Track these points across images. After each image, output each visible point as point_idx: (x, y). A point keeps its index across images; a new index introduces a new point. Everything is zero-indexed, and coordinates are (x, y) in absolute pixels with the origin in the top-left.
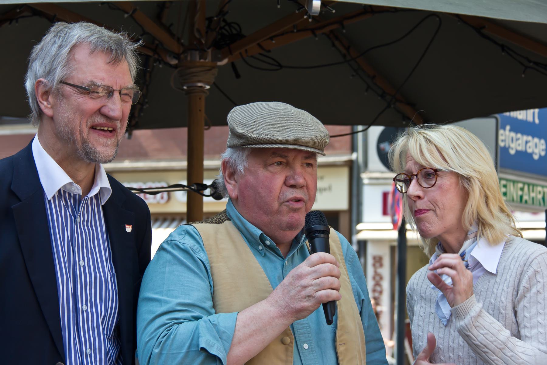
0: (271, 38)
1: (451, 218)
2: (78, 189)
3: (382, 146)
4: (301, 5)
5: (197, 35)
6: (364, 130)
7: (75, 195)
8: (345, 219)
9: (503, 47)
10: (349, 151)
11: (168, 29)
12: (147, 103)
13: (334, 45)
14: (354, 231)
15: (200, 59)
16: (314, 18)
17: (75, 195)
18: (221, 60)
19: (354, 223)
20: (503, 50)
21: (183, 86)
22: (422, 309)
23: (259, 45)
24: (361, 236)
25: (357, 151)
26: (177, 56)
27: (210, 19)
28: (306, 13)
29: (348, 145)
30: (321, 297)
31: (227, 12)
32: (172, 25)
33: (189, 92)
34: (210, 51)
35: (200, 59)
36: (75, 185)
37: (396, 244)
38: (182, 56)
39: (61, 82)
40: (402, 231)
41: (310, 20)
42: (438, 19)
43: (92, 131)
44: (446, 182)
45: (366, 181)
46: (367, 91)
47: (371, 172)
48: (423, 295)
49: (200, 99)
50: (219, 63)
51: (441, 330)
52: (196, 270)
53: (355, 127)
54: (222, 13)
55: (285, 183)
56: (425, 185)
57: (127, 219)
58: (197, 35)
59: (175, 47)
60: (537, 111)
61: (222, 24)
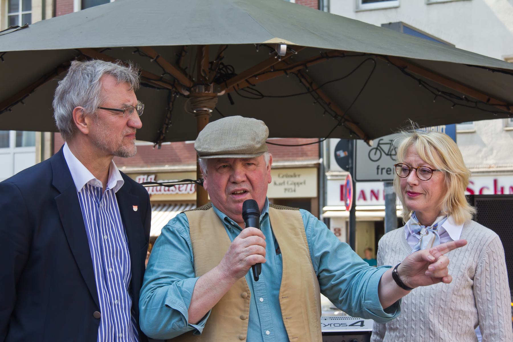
0: (255, 76)
3: (338, 153)
5: (203, 74)
7: (97, 188)
9: (420, 81)
10: (318, 157)
11: (184, 71)
12: (171, 123)
13: (301, 82)
14: (321, 212)
18: (220, 92)
19: (321, 207)
20: (420, 83)
22: (392, 258)
23: (247, 81)
24: (327, 215)
25: (323, 158)
26: (189, 89)
27: (212, 63)
28: (276, 54)
30: (250, 260)
31: (223, 57)
32: (186, 68)
33: (197, 115)
34: (212, 85)
36: (98, 180)
37: (348, 220)
38: (192, 89)
39: (98, 108)
40: (353, 212)
42: (373, 62)
44: (436, 177)
45: (329, 178)
46: (324, 113)
47: (332, 171)
48: (394, 249)
50: (219, 94)
52: (179, 246)
55: (229, 180)
56: (421, 177)
57: (135, 205)
58: (203, 74)
60: (444, 127)
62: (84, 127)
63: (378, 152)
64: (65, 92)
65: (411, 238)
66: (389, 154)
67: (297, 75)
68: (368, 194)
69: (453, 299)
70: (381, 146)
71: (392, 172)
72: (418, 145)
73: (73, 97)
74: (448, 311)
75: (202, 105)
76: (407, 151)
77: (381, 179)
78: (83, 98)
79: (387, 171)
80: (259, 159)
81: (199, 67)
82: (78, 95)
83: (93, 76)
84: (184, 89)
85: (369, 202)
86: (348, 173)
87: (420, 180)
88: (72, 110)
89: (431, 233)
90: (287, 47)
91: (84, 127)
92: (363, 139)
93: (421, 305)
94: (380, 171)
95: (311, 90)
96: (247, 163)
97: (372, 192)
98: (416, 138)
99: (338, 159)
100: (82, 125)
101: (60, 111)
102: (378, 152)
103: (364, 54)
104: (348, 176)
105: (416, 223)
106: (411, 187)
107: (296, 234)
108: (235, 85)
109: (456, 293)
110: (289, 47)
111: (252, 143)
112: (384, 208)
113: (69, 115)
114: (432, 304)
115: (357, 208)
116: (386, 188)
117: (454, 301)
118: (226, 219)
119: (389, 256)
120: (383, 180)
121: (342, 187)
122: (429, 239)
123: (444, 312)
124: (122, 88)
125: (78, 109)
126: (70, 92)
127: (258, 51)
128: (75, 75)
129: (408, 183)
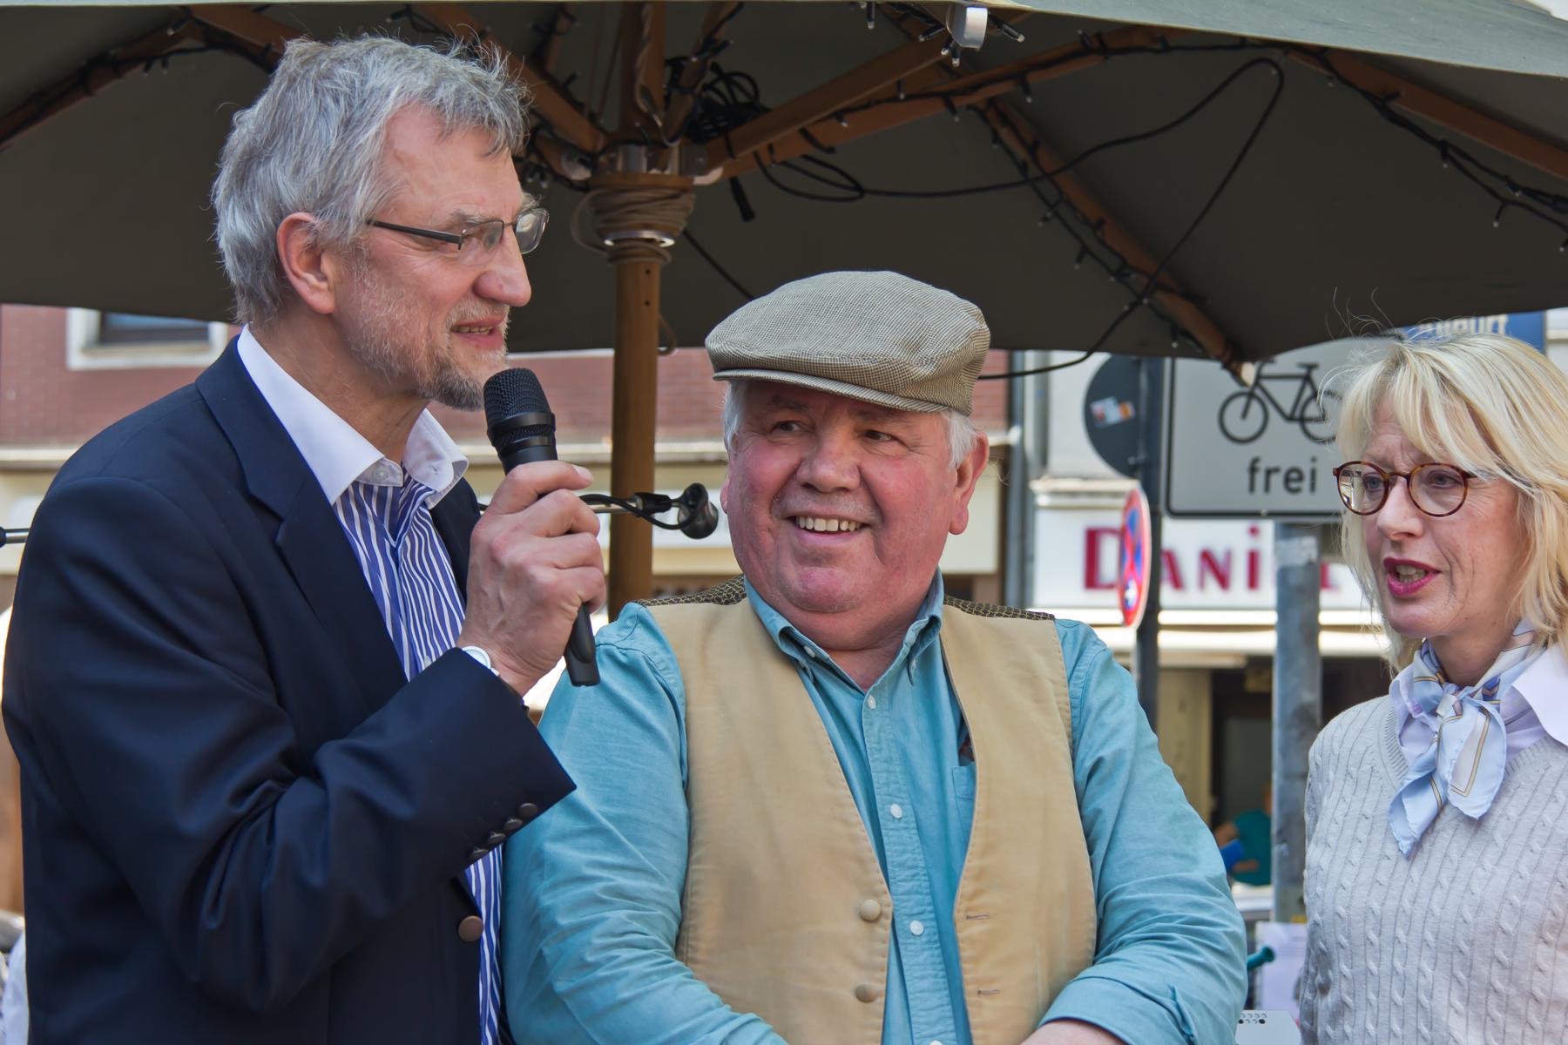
0: (839, 116)
1: (1481, 597)
2: (393, 473)
3: (1098, 407)
4: (931, 20)
6: (1044, 370)
7: (383, 490)
8: (1003, 589)
9: (1444, 148)
10: (1002, 423)
13: (996, 139)
15: (649, 168)
16: (967, 54)
17: (383, 490)
18: (704, 171)
20: (1445, 157)
21: (604, 238)
22: (1342, 806)
23: (804, 133)
25: (1022, 424)
26: (589, 160)
27: (676, 64)
28: (947, 41)
29: (1000, 407)
31: (725, 44)
32: (573, 77)
33: (617, 255)
34: (675, 145)
35: (649, 168)
38: (602, 159)
39: (368, 222)
40: (1148, 632)
41: (956, 62)
42: (1274, 72)
43: (454, 336)
44: (1484, 503)
45: (1043, 500)
46: (1079, 260)
47: (1056, 477)
49: (648, 272)
50: (699, 180)
51: (1385, 862)
53: (1018, 355)
54: (710, 45)
56: (1429, 505)
59: (585, 137)
60: (1502, 319)
61: (710, 76)
62: (318, 290)
63: (1255, 407)
64: (253, 158)
65: (1413, 730)
66: (1298, 417)
67: (983, 115)
68: (1190, 566)
69: (1540, 960)
70: (1267, 384)
71: (1306, 484)
72: (1402, 383)
73: (279, 177)
74: (1519, 1004)
75: (638, 219)
76: (1379, 409)
77: (1264, 511)
78: (314, 185)
79: (1287, 480)
80: (924, 428)
81: (630, 76)
82: (297, 170)
83: (357, 102)
84: (570, 159)
85: (1192, 594)
86: (1131, 485)
87: (1426, 517)
88: (277, 226)
89: (1471, 712)
90: (990, 17)
91: (318, 290)
92: (1218, 358)
93: (1422, 981)
94: (1260, 478)
95: (1034, 171)
96: (872, 424)
97: (1207, 558)
98: (1398, 361)
99: (1103, 438)
100: (312, 278)
101: (234, 225)
102: (1255, 407)
103: (1242, 43)
104: (1131, 499)
105: (1428, 673)
106: (1397, 545)
107: (1039, 699)
108: (761, 146)
109: (1549, 937)
110: (997, 16)
111: (897, 354)
112: (1271, 618)
113: (265, 242)
114: (1462, 976)
115: (1164, 618)
116: (1283, 544)
117: (1544, 966)
118: (786, 634)
119: (1335, 795)
120: (1272, 515)
121: (1093, 538)
122: (1465, 735)
123: (1507, 1008)
124: (464, 151)
125: (297, 223)
126: (269, 158)
127: (871, 26)
128: (290, 94)
129: (1383, 533)
